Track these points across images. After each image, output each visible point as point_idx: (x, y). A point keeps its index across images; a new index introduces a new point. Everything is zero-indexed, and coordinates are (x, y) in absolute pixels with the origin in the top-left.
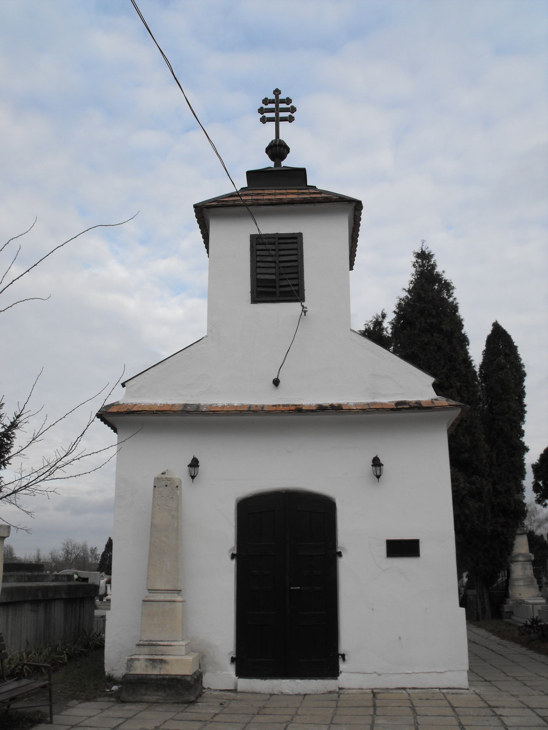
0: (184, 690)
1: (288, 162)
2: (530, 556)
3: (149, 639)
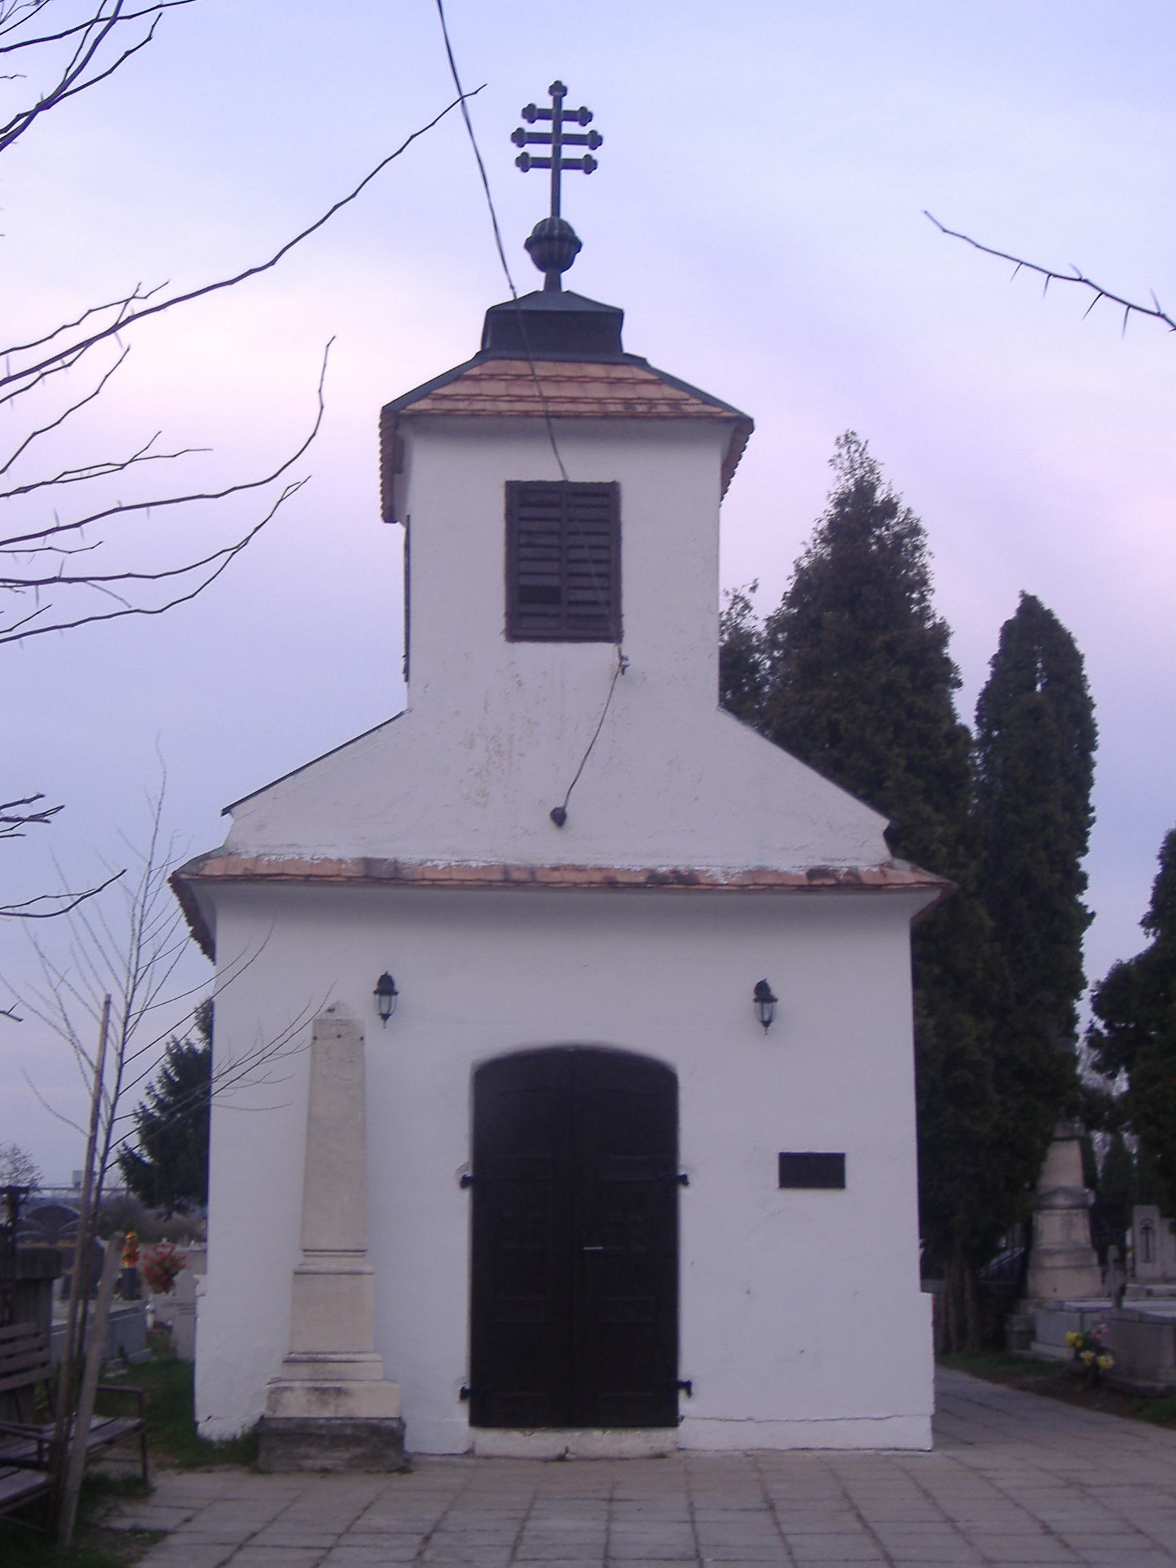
0: (379, 1446)
1: (578, 280)
2: (1085, 1195)
3: (307, 1350)
